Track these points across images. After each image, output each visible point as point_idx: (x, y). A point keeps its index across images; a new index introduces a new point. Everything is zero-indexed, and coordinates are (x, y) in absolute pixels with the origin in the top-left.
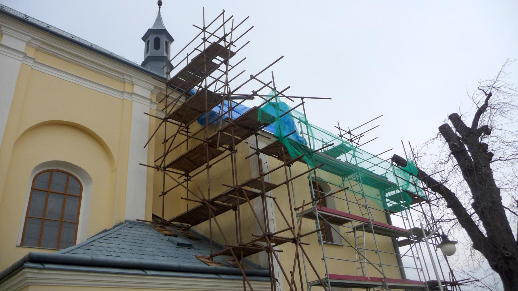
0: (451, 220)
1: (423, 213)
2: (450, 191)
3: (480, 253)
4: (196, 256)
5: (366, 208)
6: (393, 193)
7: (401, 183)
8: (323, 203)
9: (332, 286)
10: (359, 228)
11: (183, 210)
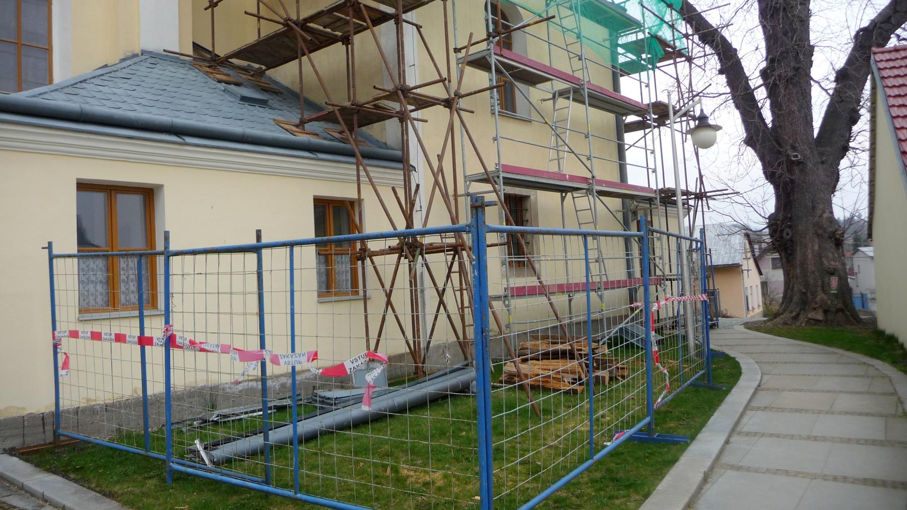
0: (720, 95)
1: (677, 79)
2: (730, 45)
3: (753, 151)
4: (274, 120)
5: (580, 59)
6: (632, 38)
7: (650, 21)
8: (507, 44)
9: (505, 184)
10: (563, 94)
11: (250, 38)
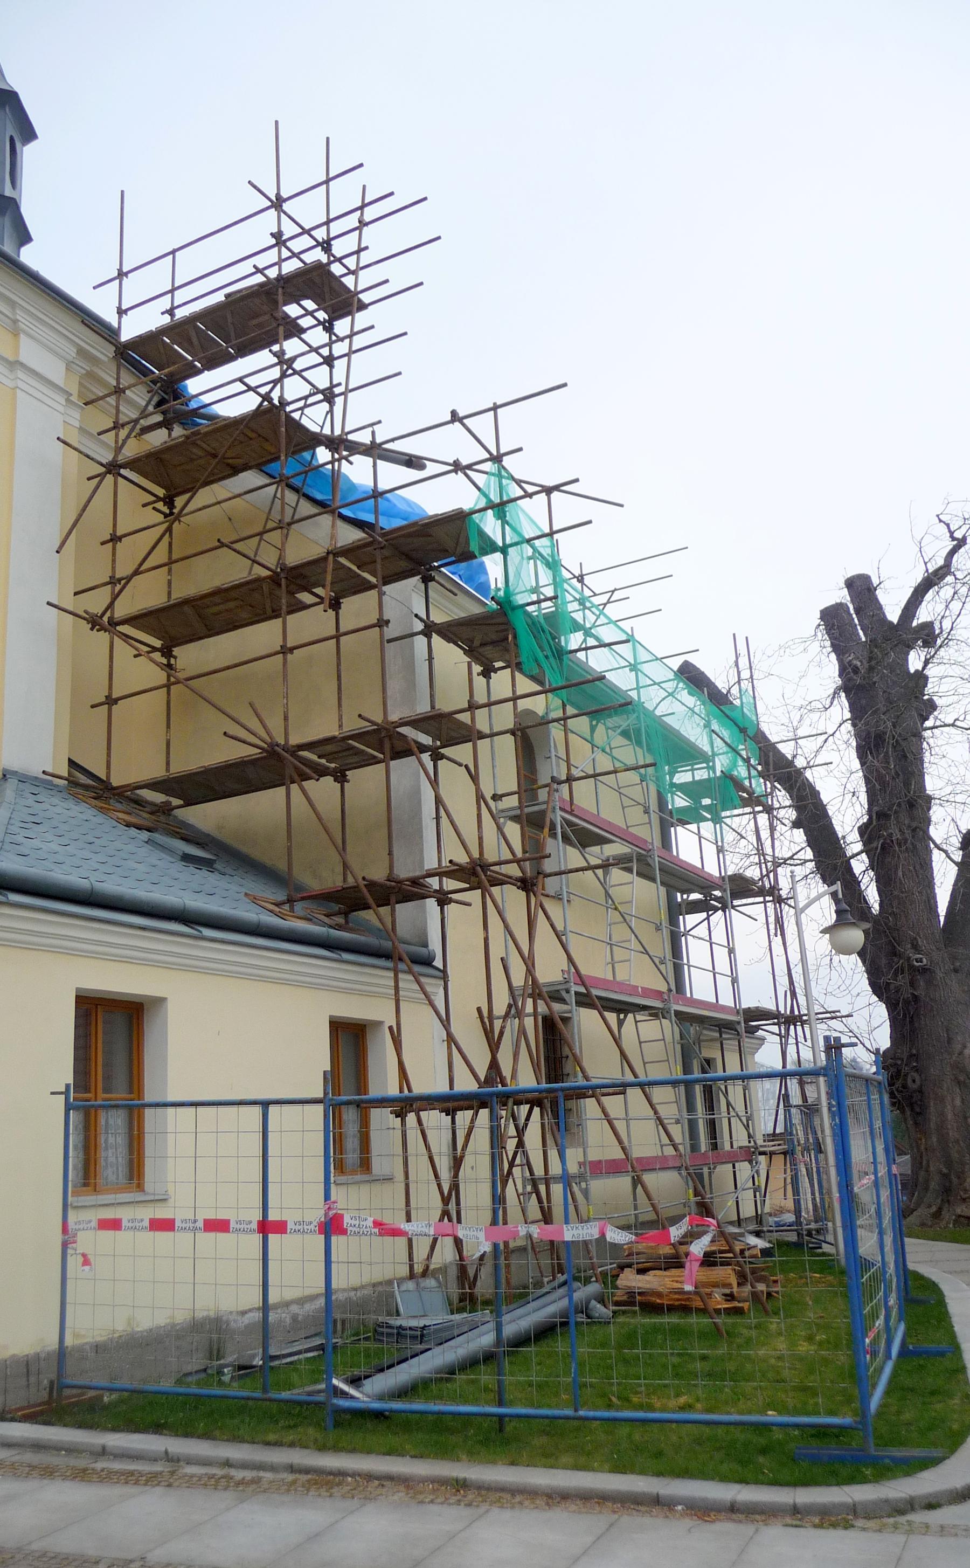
10: (623, 862)
